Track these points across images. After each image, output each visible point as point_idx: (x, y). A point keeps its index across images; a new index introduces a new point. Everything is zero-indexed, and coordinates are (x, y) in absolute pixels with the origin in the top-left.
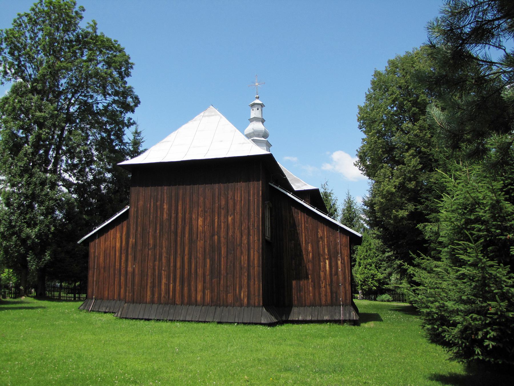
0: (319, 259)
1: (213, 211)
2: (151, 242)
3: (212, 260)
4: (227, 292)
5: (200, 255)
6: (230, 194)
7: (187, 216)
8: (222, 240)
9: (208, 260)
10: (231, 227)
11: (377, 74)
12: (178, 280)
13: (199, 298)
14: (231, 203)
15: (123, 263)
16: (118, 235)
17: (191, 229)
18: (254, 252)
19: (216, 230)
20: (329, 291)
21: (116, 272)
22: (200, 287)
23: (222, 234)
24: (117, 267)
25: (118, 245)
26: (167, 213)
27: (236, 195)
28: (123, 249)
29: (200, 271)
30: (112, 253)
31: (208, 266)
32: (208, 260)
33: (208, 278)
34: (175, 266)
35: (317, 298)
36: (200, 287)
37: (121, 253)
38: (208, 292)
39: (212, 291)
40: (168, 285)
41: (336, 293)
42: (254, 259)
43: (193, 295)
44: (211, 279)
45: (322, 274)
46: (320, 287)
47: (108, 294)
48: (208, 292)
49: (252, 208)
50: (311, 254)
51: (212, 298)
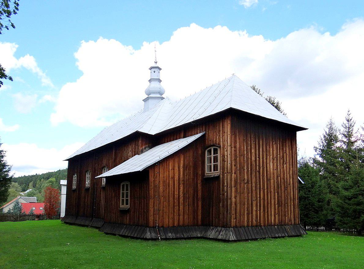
1: (277, 160)
2: (246, 177)
3: (278, 194)
5: (272, 190)
7: (265, 160)
8: (282, 181)
9: (276, 194)
12: (262, 207)
15: (181, 192)
16: (176, 166)
22: (273, 213)
24: (176, 196)
29: (273, 202)
31: (276, 197)
32: (276, 194)
33: (277, 206)
34: (260, 197)
36: (273, 213)
38: (277, 216)
44: (278, 207)
47: (169, 222)
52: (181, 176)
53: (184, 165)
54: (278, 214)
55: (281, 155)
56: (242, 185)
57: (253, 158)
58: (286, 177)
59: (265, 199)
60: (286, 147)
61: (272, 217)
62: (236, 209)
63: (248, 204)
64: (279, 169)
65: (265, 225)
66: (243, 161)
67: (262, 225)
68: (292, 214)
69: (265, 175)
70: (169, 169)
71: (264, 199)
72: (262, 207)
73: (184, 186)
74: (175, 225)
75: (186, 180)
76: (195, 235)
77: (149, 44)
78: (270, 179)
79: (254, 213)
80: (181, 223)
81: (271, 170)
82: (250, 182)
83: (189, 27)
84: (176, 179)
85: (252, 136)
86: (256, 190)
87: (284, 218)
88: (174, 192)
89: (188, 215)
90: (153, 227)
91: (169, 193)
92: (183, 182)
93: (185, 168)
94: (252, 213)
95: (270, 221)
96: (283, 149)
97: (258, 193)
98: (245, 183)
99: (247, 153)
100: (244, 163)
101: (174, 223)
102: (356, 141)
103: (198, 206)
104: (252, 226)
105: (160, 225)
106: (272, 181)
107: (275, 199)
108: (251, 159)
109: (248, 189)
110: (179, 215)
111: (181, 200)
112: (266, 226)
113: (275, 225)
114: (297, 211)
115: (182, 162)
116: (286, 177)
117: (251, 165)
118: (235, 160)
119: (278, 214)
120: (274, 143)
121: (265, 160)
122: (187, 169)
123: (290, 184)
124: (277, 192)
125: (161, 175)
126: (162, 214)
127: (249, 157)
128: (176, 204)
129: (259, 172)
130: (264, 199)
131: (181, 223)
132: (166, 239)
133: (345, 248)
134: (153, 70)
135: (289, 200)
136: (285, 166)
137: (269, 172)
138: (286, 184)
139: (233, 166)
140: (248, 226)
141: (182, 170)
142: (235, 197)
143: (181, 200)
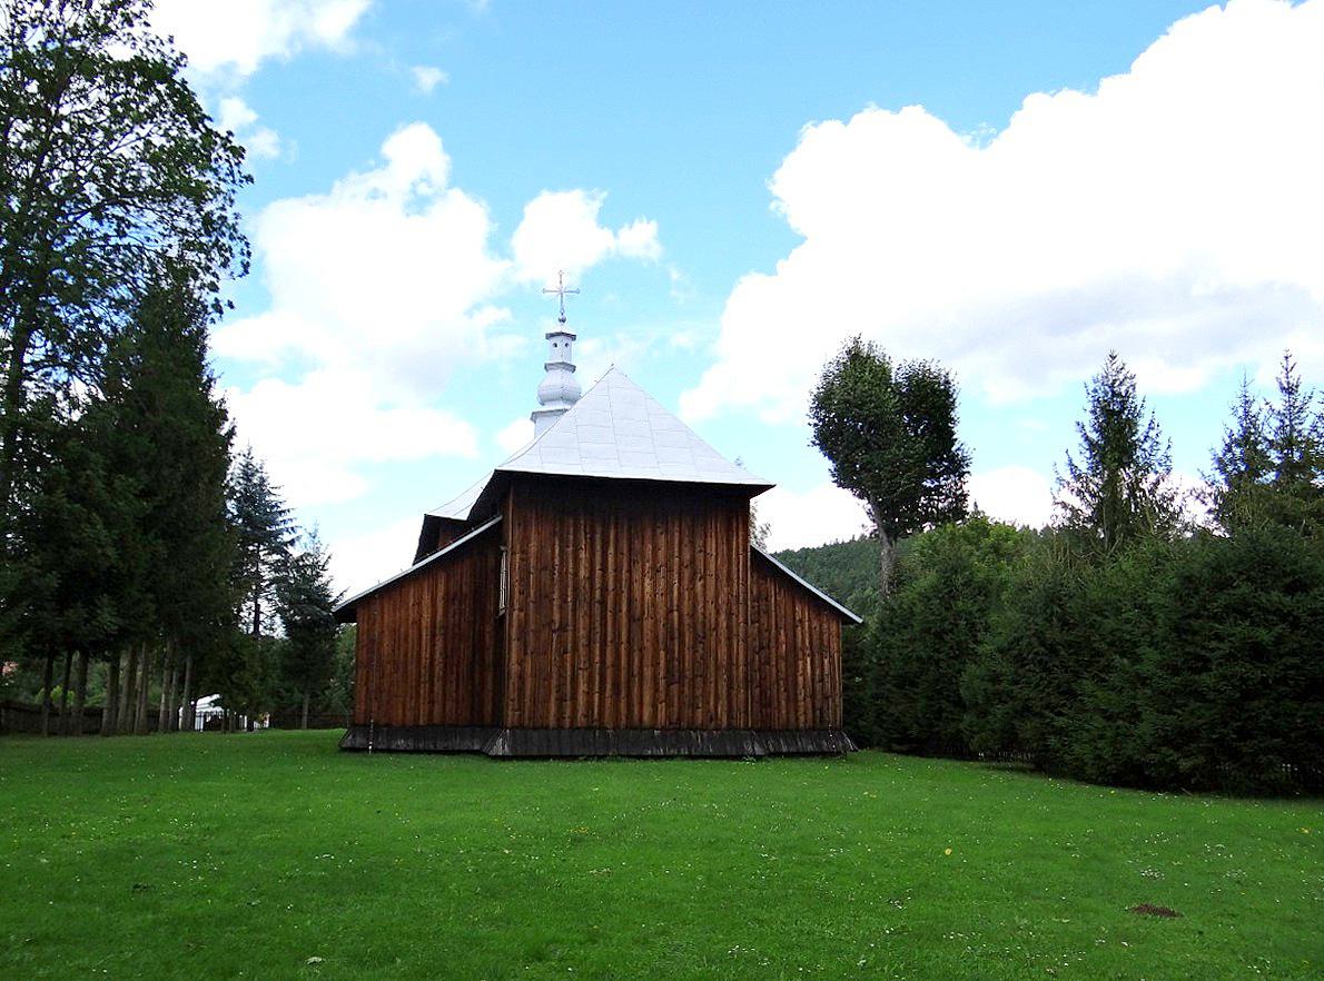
0: (796, 656)
1: (670, 571)
2: (557, 617)
3: (669, 651)
4: (694, 707)
6: (700, 543)
7: (625, 575)
8: (687, 620)
10: (700, 598)
11: (787, 259)
12: (609, 686)
13: (646, 718)
14: (700, 556)
15: (438, 653)
16: (427, 598)
17: (630, 600)
18: (738, 641)
19: (675, 602)
20: (810, 706)
21: (423, 671)
22: (647, 699)
23: (686, 610)
24: (425, 662)
25: (426, 617)
26: (585, 568)
27: (709, 544)
28: (438, 625)
29: (648, 672)
30: (412, 634)
31: (662, 662)
33: (662, 682)
34: (603, 661)
35: (792, 720)
36: (647, 699)
37: (433, 636)
38: (662, 707)
39: (669, 705)
40: (589, 694)
41: (821, 709)
42: (738, 654)
43: (636, 712)
44: (668, 685)
45: (801, 679)
46: (796, 701)
47: (404, 715)
48: (662, 707)
49: (734, 568)
50: (784, 646)
51: (668, 717)
52: (439, 618)
53: (447, 593)
54: (665, 701)
55: (687, 556)
56: (544, 635)
57: (583, 573)
58: (700, 610)
59: (620, 664)
60: (706, 537)
61: (645, 708)
62: (521, 690)
63: (561, 676)
64: (676, 593)
65: (619, 727)
66: (548, 582)
67: (609, 724)
68: (723, 702)
69: (624, 609)
70: (408, 604)
71: (616, 665)
72: (609, 686)
73: (445, 640)
74: (421, 723)
75: (451, 627)
76: (466, 745)
77: (1223, 8)
78: (641, 619)
79: (581, 699)
80: (437, 720)
81: (647, 597)
82: (570, 628)
83: (846, 123)
84: (424, 624)
85: (582, 522)
86: (589, 645)
87: (687, 712)
88: (419, 654)
89: (457, 701)
90: (365, 725)
91: (406, 655)
92: (442, 631)
93: (448, 599)
94: (574, 698)
95: (636, 718)
96: (692, 543)
97: (597, 652)
98: (554, 631)
99: (561, 563)
100: (552, 585)
101: (417, 718)
102: (1065, 505)
103: (483, 682)
104: (573, 728)
105: (383, 721)
106: (648, 624)
107: (655, 664)
108: (576, 574)
109: (561, 642)
110: (432, 702)
111: (438, 670)
112: (622, 727)
113: (653, 728)
114: (742, 696)
115: (441, 587)
116: (700, 610)
117: (575, 589)
118: (524, 580)
119: (665, 701)
120: (659, 531)
121: (625, 575)
122: (456, 602)
123: (716, 629)
124: (666, 649)
125: (386, 616)
126: (140, 660)
127: (571, 570)
128: (425, 676)
129: (603, 602)
130: (616, 665)
131: (437, 720)
132: (389, 751)
133: (1251, 855)
134: (556, 340)
135: (712, 669)
136: (699, 584)
137: (638, 604)
138: (699, 627)
139: (517, 594)
140: (560, 727)
141: (440, 605)
142: (521, 663)
143: (438, 670)
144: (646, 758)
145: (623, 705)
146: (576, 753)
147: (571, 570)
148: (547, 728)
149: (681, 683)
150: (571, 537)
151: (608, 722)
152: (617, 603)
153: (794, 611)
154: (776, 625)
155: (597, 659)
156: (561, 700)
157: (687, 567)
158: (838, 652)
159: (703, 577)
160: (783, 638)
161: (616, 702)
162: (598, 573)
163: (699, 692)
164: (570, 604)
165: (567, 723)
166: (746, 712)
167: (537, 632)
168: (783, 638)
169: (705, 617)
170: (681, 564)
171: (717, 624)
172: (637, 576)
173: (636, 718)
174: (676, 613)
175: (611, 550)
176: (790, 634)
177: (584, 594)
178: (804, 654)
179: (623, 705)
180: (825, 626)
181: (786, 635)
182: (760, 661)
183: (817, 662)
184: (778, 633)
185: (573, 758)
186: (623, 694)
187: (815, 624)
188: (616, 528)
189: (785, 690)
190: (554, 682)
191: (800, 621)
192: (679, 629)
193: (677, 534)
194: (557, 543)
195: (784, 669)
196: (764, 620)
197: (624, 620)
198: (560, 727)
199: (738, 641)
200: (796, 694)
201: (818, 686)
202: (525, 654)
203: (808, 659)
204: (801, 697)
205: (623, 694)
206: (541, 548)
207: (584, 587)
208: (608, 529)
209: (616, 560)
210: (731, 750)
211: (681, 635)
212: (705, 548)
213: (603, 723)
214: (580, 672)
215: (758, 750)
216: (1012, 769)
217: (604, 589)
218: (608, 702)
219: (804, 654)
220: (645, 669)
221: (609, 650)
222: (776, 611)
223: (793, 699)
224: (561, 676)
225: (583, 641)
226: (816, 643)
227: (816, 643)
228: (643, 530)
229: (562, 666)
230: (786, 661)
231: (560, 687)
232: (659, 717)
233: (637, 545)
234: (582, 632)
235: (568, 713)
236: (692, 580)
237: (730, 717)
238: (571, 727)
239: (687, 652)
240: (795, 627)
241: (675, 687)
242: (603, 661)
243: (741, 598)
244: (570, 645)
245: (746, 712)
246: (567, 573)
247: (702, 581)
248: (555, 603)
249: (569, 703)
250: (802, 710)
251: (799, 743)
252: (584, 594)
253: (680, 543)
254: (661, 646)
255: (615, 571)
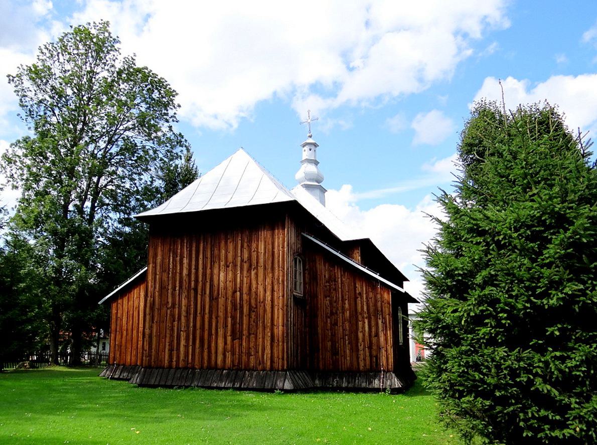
1: (235, 266)
2: (170, 300)
4: (249, 355)
6: (254, 245)
7: (208, 271)
8: (245, 297)
14: (254, 255)
17: (211, 286)
19: (238, 286)
20: (368, 354)
23: (245, 290)
34: (195, 326)
35: (355, 363)
38: (228, 355)
39: (233, 354)
40: (187, 347)
45: (360, 335)
46: (358, 350)
51: (233, 361)
55: (246, 256)
57: (185, 272)
61: (218, 355)
63: (172, 336)
69: (208, 292)
78: (217, 298)
79: (182, 349)
85: (185, 241)
87: (244, 358)
95: (213, 363)
96: (249, 247)
99: (173, 267)
104: (177, 368)
106: (221, 301)
108: (181, 273)
112: (268, 369)
136: (253, 273)
140: (170, 367)
144: (213, 388)
145: (206, 354)
146: (173, 384)
147: (178, 271)
148: (163, 368)
149: (241, 339)
150: (179, 251)
151: (197, 364)
152: (204, 289)
153: (355, 287)
154: (342, 297)
155: (192, 324)
156: (171, 350)
157: (246, 262)
158: (389, 315)
159: (257, 268)
160: (347, 306)
161: (202, 352)
162: (193, 271)
163: (252, 345)
164: (178, 291)
165: (206, 364)
166: (283, 359)
167: (160, 309)
168: (347, 306)
169: (257, 294)
170: (242, 261)
171: (264, 299)
172: (216, 271)
173: (213, 363)
174: (238, 293)
175: (201, 256)
176: (353, 305)
177: (185, 285)
178: (363, 318)
179: (206, 354)
180: (379, 296)
181: (350, 304)
182: (331, 323)
183: (373, 323)
184: (343, 303)
185: (171, 387)
186: (206, 346)
187: (371, 295)
188: (204, 242)
189: (349, 343)
190: (168, 340)
191: (360, 294)
192: (240, 304)
193: (240, 242)
194: (171, 255)
195: (347, 328)
196: (334, 294)
197: (207, 300)
198: (170, 367)
199: (278, 309)
200: (357, 346)
201: (374, 340)
202: (153, 322)
203: (366, 321)
204: (361, 348)
205: (206, 346)
206: (163, 259)
207: (185, 280)
208: (200, 243)
209: (203, 263)
210: (268, 385)
211: (242, 307)
212: (258, 249)
213: (194, 366)
214: (182, 333)
215: (288, 385)
216: (106, 415)
217: (197, 281)
218: (197, 351)
219: (363, 318)
220: (219, 330)
221: (198, 318)
222: (341, 288)
223: (355, 349)
224: (172, 336)
225: (184, 313)
226: (372, 309)
227: (372, 309)
228: (219, 243)
229: (172, 330)
230: (350, 322)
231: (171, 345)
232: (227, 362)
233: (216, 252)
234: (184, 308)
235: (206, 357)
236: (249, 270)
237: (272, 361)
238: (176, 367)
239: (245, 318)
240: (356, 298)
241: (237, 342)
242: (195, 326)
243: (280, 280)
244: (177, 316)
245: (283, 359)
246: (176, 273)
247: (255, 271)
248: (169, 291)
249: (175, 352)
250: (362, 357)
251: (357, 381)
252: (185, 285)
253: (242, 246)
254: (229, 315)
255: (203, 269)
